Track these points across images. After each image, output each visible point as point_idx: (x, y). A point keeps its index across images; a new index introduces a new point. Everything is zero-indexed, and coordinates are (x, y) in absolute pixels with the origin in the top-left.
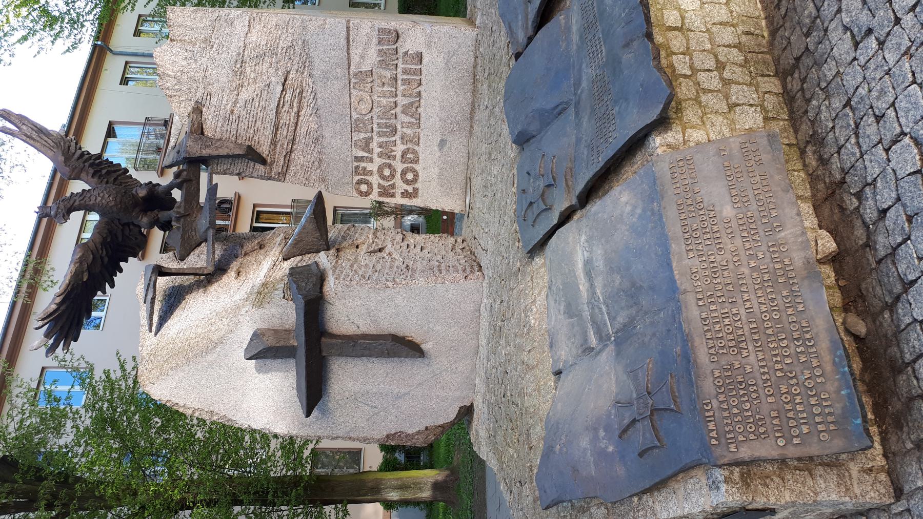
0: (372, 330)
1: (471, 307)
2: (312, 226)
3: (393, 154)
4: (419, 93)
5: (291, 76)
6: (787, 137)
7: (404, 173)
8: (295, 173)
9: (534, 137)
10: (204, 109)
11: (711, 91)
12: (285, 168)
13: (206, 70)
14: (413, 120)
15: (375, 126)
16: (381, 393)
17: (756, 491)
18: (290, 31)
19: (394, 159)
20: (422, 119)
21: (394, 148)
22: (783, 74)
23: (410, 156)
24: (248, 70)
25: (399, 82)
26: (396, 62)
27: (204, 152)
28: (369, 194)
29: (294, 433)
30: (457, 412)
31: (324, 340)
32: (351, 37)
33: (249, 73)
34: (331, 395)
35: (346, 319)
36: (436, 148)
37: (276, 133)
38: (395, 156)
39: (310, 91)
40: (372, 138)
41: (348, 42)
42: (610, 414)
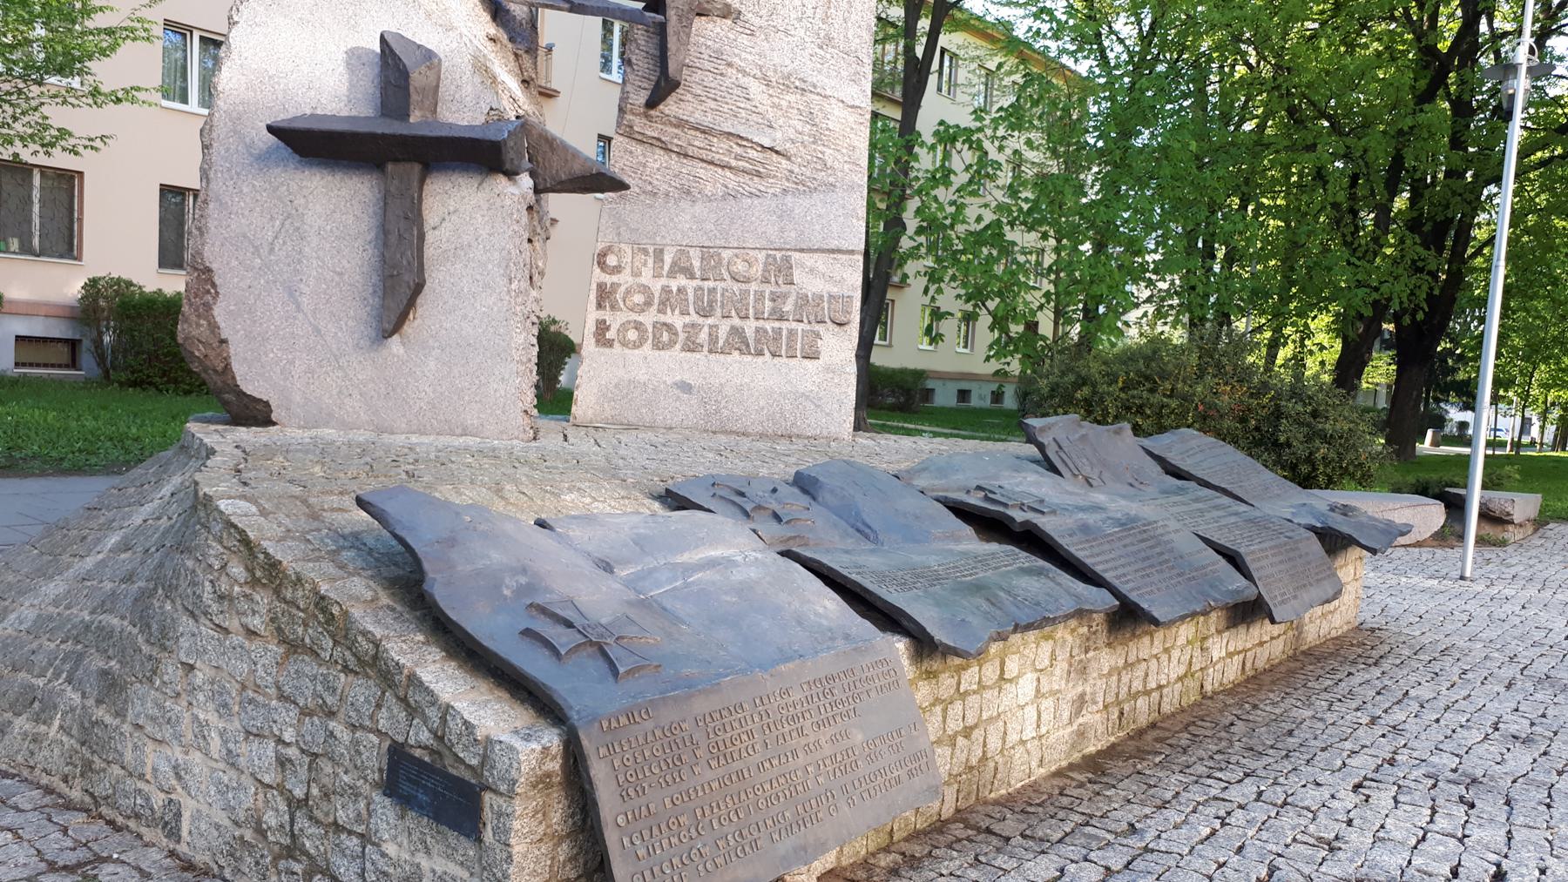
0: (429, 252)
1: (471, 420)
2: (577, 169)
3: (669, 310)
4: (760, 353)
5: (784, 162)
6: (900, 829)
7: (638, 326)
8: (631, 152)
9: (814, 499)
10: (729, 22)
11: (944, 718)
12: (640, 138)
13: (786, 32)
14: (721, 343)
15: (711, 284)
16: (300, 261)
17: (528, 798)
18: (846, 167)
19: (659, 311)
20: (722, 356)
21: (677, 312)
22: (960, 815)
23: (665, 337)
24: (792, 98)
25: (777, 324)
26: (805, 320)
27: (673, 12)
28: (602, 269)
29: (220, 103)
30: (258, 396)
31: (417, 168)
32: (840, 256)
33: (787, 98)
34: (299, 172)
35: (452, 209)
36: (678, 378)
37: (697, 129)
38: (665, 313)
39: (763, 189)
40: (692, 277)
41: (833, 251)
42: (551, 592)
